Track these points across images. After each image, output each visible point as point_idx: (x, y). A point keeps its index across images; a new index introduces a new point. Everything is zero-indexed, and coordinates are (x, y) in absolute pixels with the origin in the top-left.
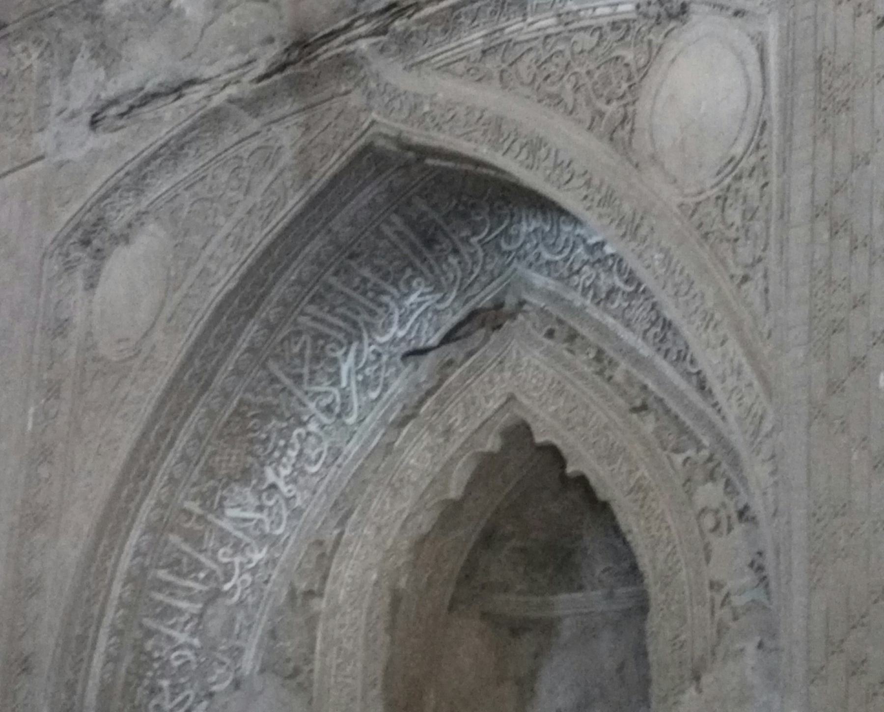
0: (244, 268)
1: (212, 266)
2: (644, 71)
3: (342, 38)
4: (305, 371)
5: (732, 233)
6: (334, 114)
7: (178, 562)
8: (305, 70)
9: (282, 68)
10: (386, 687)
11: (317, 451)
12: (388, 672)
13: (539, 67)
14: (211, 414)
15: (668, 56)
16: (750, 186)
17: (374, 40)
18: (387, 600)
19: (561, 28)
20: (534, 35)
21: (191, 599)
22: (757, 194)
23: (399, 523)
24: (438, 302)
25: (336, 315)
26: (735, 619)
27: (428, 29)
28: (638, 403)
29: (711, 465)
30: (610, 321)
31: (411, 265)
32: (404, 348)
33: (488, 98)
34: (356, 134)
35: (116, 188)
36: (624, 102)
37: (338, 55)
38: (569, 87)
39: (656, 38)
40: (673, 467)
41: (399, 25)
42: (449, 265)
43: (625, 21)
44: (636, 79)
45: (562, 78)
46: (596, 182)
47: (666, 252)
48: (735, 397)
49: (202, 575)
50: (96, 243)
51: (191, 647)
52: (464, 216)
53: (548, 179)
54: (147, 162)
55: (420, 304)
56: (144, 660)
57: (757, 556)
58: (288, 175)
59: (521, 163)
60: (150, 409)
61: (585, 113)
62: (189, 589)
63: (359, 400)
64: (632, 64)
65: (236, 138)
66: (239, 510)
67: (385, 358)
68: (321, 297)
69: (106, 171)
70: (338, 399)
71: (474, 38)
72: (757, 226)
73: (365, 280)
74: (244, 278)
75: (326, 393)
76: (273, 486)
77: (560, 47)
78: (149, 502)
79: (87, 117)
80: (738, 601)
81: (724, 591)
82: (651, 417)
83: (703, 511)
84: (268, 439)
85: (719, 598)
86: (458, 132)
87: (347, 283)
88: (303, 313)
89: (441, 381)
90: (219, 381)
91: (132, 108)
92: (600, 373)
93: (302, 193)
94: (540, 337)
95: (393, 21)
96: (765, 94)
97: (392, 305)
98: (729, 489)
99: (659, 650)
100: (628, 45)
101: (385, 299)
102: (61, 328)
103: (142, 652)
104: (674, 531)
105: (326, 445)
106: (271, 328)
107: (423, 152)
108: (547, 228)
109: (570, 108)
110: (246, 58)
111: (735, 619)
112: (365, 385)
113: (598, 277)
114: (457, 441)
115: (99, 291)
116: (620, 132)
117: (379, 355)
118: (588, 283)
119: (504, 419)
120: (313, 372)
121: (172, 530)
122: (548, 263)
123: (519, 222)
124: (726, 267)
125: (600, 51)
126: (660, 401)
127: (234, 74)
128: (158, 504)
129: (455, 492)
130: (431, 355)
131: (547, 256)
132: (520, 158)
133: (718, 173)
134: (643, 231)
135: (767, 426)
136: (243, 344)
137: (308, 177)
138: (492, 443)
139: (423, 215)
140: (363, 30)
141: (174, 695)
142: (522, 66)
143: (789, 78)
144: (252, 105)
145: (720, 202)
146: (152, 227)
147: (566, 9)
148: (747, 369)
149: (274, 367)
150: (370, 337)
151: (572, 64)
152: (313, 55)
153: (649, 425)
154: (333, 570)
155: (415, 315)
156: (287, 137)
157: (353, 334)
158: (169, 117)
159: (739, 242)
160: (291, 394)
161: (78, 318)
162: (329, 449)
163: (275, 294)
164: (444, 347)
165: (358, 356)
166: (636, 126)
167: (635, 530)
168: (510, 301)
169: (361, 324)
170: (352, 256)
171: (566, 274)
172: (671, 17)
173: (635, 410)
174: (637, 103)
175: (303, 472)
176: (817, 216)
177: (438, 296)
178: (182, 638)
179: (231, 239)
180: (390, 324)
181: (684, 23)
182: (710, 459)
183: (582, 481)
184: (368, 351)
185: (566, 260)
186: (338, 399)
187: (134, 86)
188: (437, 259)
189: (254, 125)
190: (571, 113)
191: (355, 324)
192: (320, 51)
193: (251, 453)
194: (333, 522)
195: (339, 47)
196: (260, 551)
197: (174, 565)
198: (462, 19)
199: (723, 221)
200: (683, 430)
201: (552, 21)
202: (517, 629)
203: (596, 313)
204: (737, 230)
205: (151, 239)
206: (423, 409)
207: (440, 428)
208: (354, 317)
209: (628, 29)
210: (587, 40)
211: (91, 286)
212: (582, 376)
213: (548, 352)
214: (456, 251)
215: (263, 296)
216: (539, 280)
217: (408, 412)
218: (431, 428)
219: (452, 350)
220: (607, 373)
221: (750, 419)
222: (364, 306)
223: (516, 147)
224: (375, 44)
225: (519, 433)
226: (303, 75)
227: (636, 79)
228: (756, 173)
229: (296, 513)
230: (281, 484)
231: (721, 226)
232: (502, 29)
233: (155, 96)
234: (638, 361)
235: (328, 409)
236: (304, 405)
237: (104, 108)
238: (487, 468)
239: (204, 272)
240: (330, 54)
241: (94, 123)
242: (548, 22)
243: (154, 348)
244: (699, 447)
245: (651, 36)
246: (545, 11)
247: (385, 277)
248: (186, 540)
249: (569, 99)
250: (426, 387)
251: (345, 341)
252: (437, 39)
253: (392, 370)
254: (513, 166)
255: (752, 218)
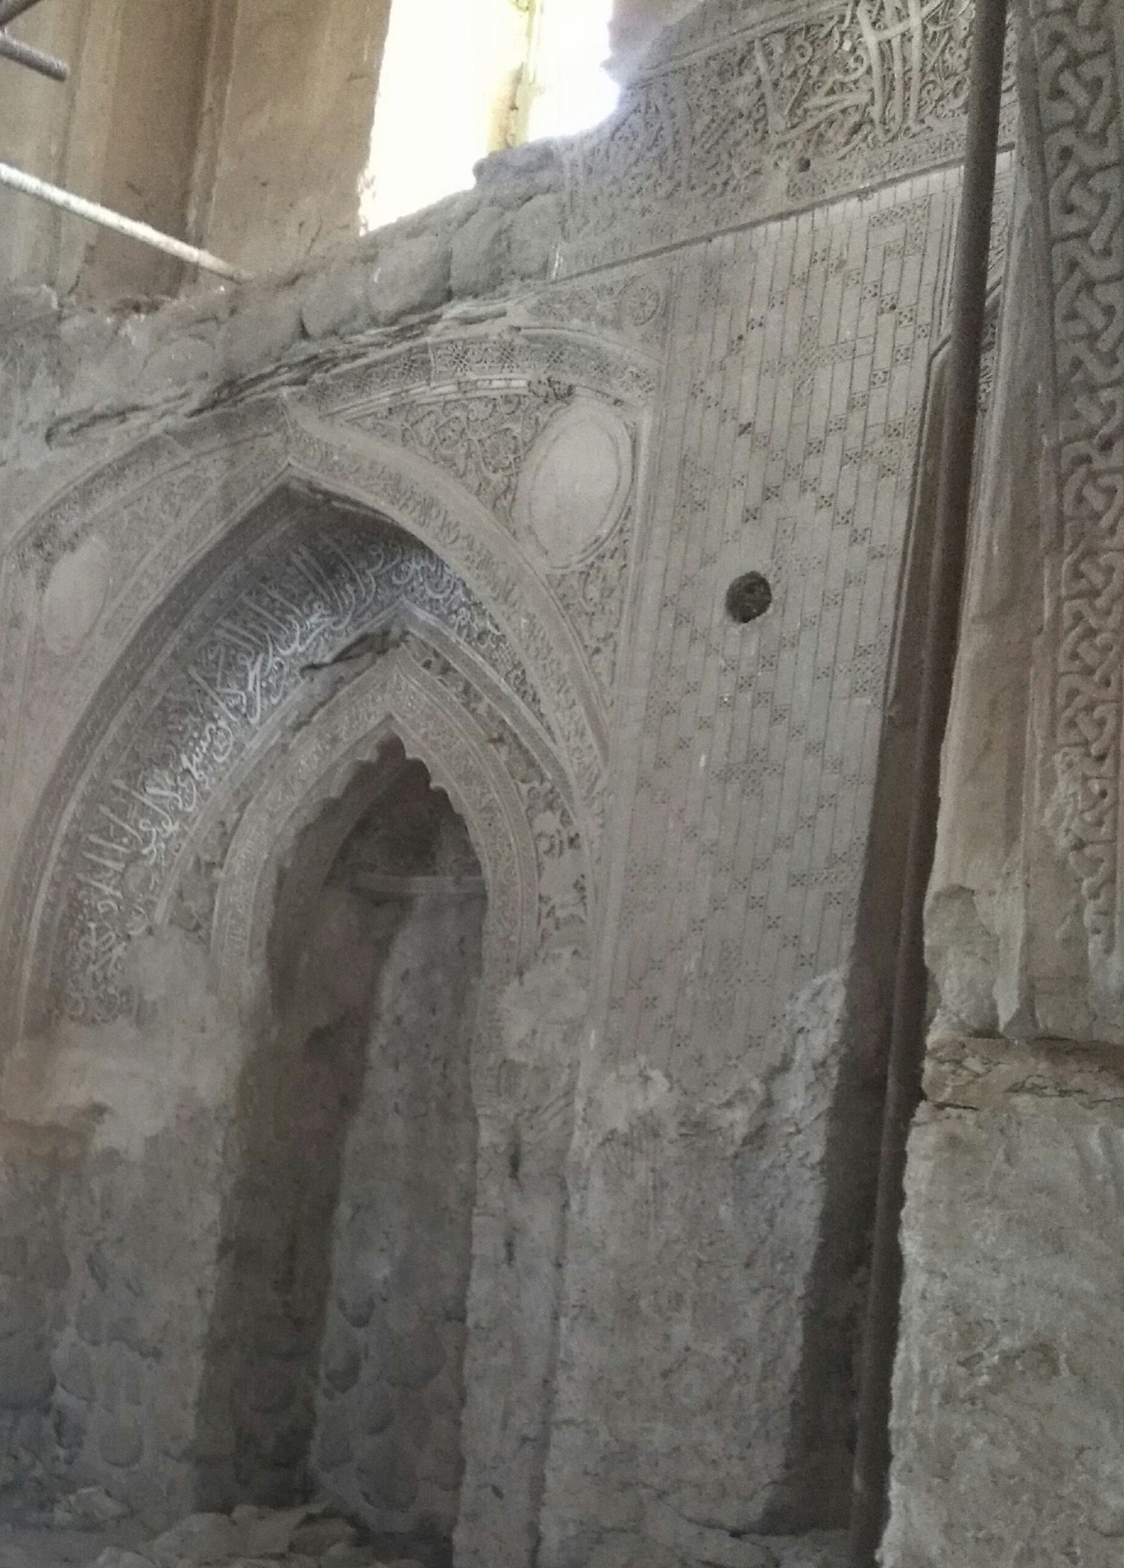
0: (172, 585)
1: (145, 582)
2: (529, 445)
3: (265, 384)
4: (219, 676)
5: (590, 609)
6: (256, 453)
7: (107, 829)
8: (233, 410)
9: (214, 404)
10: (269, 947)
11: (224, 744)
12: (271, 936)
13: (437, 431)
14: (138, 709)
15: (551, 433)
16: (610, 566)
17: (294, 389)
18: (274, 880)
19: (460, 396)
20: (435, 399)
21: (116, 860)
22: (616, 574)
23: (289, 814)
24: (334, 624)
25: (246, 629)
26: (557, 928)
27: (343, 383)
28: (495, 735)
29: (551, 796)
30: (479, 659)
31: (315, 591)
32: (304, 662)
33: (390, 454)
34: (273, 476)
35: (64, 500)
36: (508, 472)
37: (262, 401)
38: (463, 451)
39: (544, 418)
40: (519, 793)
41: (317, 377)
42: (346, 592)
43: (518, 395)
44: (521, 453)
45: (457, 442)
46: (477, 545)
47: (531, 617)
48: (577, 755)
49: (125, 840)
50: (48, 547)
51: (113, 897)
52: (361, 550)
53: (436, 537)
54: (93, 480)
55: (318, 625)
56: (76, 906)
57: (581, 879)
58: (212, 506)
59: (415, 521)
60: (88, 702)
61: (473, 480)
62: (114, 851)
63: (262, 703)
64: (520, 438)
65: (169, 466)
66: (158, 789)
67: (286, 669)
68: (236, 613)
69: (57, 485)
70: (244, 701)
71: (382, 397)
72: (612, 605)
73: (273, 600)
74: (169, 598)
75: (235, 696)
76: (188, 771)
77: (457, 413)
78: (86, 778)
79: (42, 430)
80: (560, 913)
81: (551, 904)
82: (504, 750)
83: (540, 835)
84: (184, 732)
85: (545, 909)
86: (363, 483)
87: (258, 602)
88: (219, 626)
89: (331, 697)
90: (145, 681)
91: (81, 426)
92: (466, 705)
93: (223, 523)
94: (419, 665)
95: (313, 372)
96: (633, 480)
97: (294, 622)
98: (564, 819)
99: (492, 946)
100: (517, 420)
101: (290, 617)
102: (16, 622)
103: (75, 899)
104: (514, 849)
105: (232, 739)
106: (191, 638)
107: (329, 496)
108: (433, 569)
109: (461, 473)
110: (183, 391)
111: (557, 928)
112: (268, 691)
113: (472, 619)
114: (342, 748)
115: (48, 591)
116: (503, 500)
117: (281, 666)
118: (463, 623)
119: (383, 733)
120: (224, 676)
121: (103, 802)
122: (431, 600)
123: (409, 560)
124: (582, 640)
125: (492, 421)
126: (515, 736)
127: (171, 405)
128: (93, 781)
129: (335, 793)
130: (325, 670)
131: (430, 593)
132: (413, 515)
133: (584, 551)
134: (514, 596)
135: (599, 787)
136: (168, 650)
137: (228, 509)
138: (369, 755)
139: (327, 547)
140: (285, 377)
141: (99, 935)
142: (421, 427)
143: (656, 476)
144: (185, 437)
145: (583, 577)
146: (94, 539)
147: (466, 379)
148: (589, 731)
149: (193, 671)
150: (275, 649)
151: (467, 431)
152: (239, 397)
153: (503, 755)
154: (233, 846)
155: (314, 634)
156: (214, 471)
157: (260, 649)
158: (113, 442)
159: (595, 617)
160: (206, 694)
161: (31, 614)
162: (235, 743)
163: (197, 610)
164: (335, 666)
165: (264, 665)
166: (518, 495)
167: (482, 842)
168: (396, 632)
169: (268, 638)
170: (264, 580)
171: (446, 612)
172: (558, 397)
173: (493, 741)
174: (521, 475)
175: (212, 761)
176: (666, 605)
177: (335, 618)
178: (108, 890)
179: (161, 558)
180: (293, 640)
181: (568, 404)
182: (551, 791)
183: (442, 795)
184: (272, 662)
185: (446, 600)
186: (244, 701)
187: (85, 406)
188: (337, 587)
189: (186, 455)
190: (461, 477)
191: (262, 638)
192: (247, 393)
193: (170, 742)
194: (235, 807)
195: (264, 391)
196: (173, 823)
197: (103, 832)
198: (373, 379)
199: (584, 597)
200: (531, 764)
201: (453, 388)
202: (379, 901)
203: (467, 650)
204: (595, 605)
205: (93, 548)
206: (315, 718)
207: (328, 736)
208: (260, 630)
209: (519, 403)
210: (479, 410)
211: (42, 586)
212: (452, 703)
213: (423, 680)
214: (353, 580)
215: (186, 611)
216: (422, 615)
217: (302, 719)
218: (320, 736)
219: (341, 669)
220: (473, 705)
221: (587, 776)
222: (271, 623)
223: (411, 503)
224: (294, 394)
225: (392, 748)
226: (231, 415)
227: (522, 450)
228: (617, 555)
229: (204, 795)
230: (193, 770)
231: (582, 600)
232: (407, 391)
233: (102, 417)
234: (500, 698)
235: (236, 710)
236: (217, 704)
237: (57, 424)
238: (364, 774)
239: (138, 588)
240: (254, 398)
241: (49, 437)
242: (448, 389)
243: (93, 649)
244: (543, 779)
245: (538, 414)
246: (446, 379)
247: (292, 598)
248: (113, 811)
249: (461, 465)
250: (321, 699)
251: (253, 652)
252: (351, 395)
253: (292, 680)
254: (406, 520)
255: (608, 596)
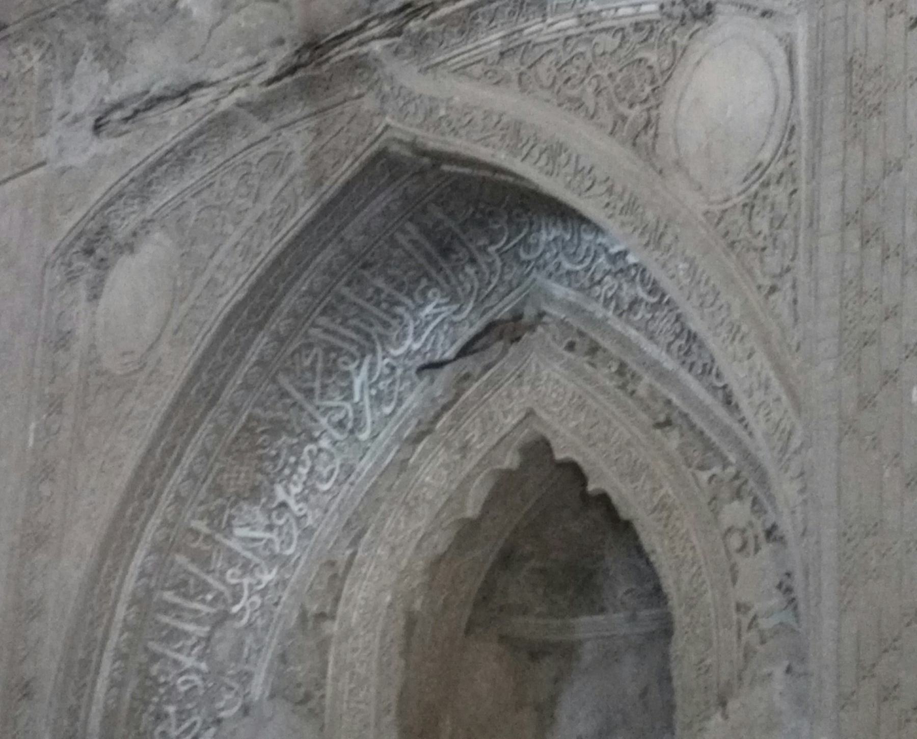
0: (253, 278)
1: (220, 277)
2: (668, 73)
3: (355, 40)
4: (317, 385)
5: (759, 242)
6: (346, 118)
7: (185, 583)
8: (317, 73)
9: (293, 70)
10: (401, 714)
11: (329, 468)
12: (403, 698)
13: (559, 70)
14: (219, 430)
15: (693, 58)
16: (778, 193)
17: (387, 41)
18: (402, 623)
19: (582, 29)
20: (554, 36)
21: (198, 622)
22: (786, 201)
23: (414, 543)
24: (455, 313)
25: (348, 327)
26: (763, 642)
27: (444, 30)
28: (662, 418)
29: (737, 483)
30: (632, 333)
31: (426, 275)
32: (419, 361)
33: (507, 101)
34: (369, 139)
35: (120, 195)
36: (647, 106)
37: (351, 57)
38: (590, 90)
39: (681, 39)
40: (698, 485)
41: (414, 25)
42: (466, 275)
43: (648, 22)
44: (660, 82)
45: (583, 80)
46: (618, 189)
47: (691, 262)
48: (762, 412)
49: (209, 597)
50: (100, 252)
51: (198, 671)
52: (482, 224)
53: (568, 185)
54: (153, 168)
55: (435, 316)
56: (149, 685)
57: (785, 578)
58: (299, 182)
59: (541, 169)
60: (156, 425)
61: (607, 118)
62: (197, 611)
63: (373, 415)
64: (656, 66)
65: (245, 143)
66: (248, 529)
67: (399, 371)
68: (333, 308)
69: (110, 178)
70: (351, 415)
71: (492, 40)
72: (786, 235)
73: (378, 291)
74: (253, 289)
75: (339, 408)
76: (283, 505)
77: (581, 49)
78: (155, 521)
79: (90, 121)
80: (766, 624)
81: (751, 614)
82: (675, 433)
83: (730, 530)
84: (278, 456)
85: (746, 621)
86: (475, 137)
87: (360, 294)
88: (314, 325)
89: (458, 396)
90: (227, 395)
91: (136, 112)
92: (623, 387)
93: (313, 200)
94: (561, 350)
95: (407, 22)
96: (794, 98)
97: (407, 316)
98: (756, 508)
99: (683, 675)
100: (652, 47)
101: (400, 310)
102: (63, 340)
103: (147, 677)
104: (699, 551)
105: (338, 462)
106: (281, 340)
107: (439, 158)
108: (568, 237)
109: (591, 112)
110: (255, 60)
111: (763, 642)
112: (378, 400)
113: (620, 287)
114: (474, 458)
115: (102, 302)
116: (643, 137)
117: (393, 369)
118: (610, 294)
119: (523, 435)
120: (324, 387)
121: (178, 551)
122: (569, 273)
123: (539, 230)
124: (753, 277)
125: (622, 53)
126: (685, 416)
127: (242, 77)
128: (164, 523)
129: (471, 511)
130: (447, 368)
131: (567, 266)
132: (539, 164)
133: (745, 180)
134: (667, 240)
135: (796, 442)
136: (252, 357)
137: (319, 183)
138: (510, 460)
139: (439, 223)
140: (376, 31)
141: (180, 722)
142: (541, 69)
143: (818, 81)
144: (262, 109)
145: (747, 210)
146: (157, 236)
147: (587, 9)
148: (775, 383)
149: (284, 381)
150: (384, 349)
151: (594, 66)
152: (325, 57)
153: (673, 441)
154: (346, 592)
155: (431, 327)
156: (298, 142)
157: (367, 347)
158: (176, 122)
159: (767, 252)
160: (302, 409)
161: (81, 330)
162: (342, 466)
163: (286, 305)
164: (460, 360)
165: (371, 370)
166: (660, 131)
167: (659, 550)
168: (529, 312)
169: (375, 337)
170: (365, 266)
171: (587, 284)
172: (696, 17)
173: (659, 425)
174: (661, 107)
175: (314, 490)
176: (848, 224)
177: (455, 307)
178: (189, 662)
179: (240, 248)
180: (405, 336)
181: (710, 23)
182: (737, 476)
183: (603, 499)
184: (382, 364)
185: (587, 269)
186: (351, 415)
187: (139, 89)
188: (454, 269)
189: (264, 129)
190: (592, 117)
191: (368, 337)
192: (332, 53)
193: (260, 470)
194: (346, 542)
195: (351, 48)
196: (270, 571)
197: (180, 587)
198: (479, 20)
199: (750, 229)
200: (708, 446)
201: (573, 22)
202: (536, 653)
203: (618, 325)
204: (765, 238)
205: (156, 248)
206: (439, 425)
207: (457, 444)
208: (368, 329)
209: (652, 30)
210: (609, 42)
211: (94, 297)
212: (604, 390)
213: (568, 365)
214: (473, 261)
215: (273, 308)
216: (559, 290)
217: (423, 428)
218: (447, 445)
219: (469, 364)
220: (630, 387)
221: (778, 435)
222: (378, 318)
223: (536, 152)
224: (389, 46)
225: (538, 450)
226: (314, 78)
227: (660, 82)
228: (784, 180)
229: (307, 532)
230: (291, 502)
231: (748, 235)
232: (521, 30)
233: (161, 99)
234: (662, 375)
235: (341, 425)
236: (316, 421)
237: (108, 113)
238: (505, 486)
239: (212, 282)
240: (342, 56)
241: (98, 127)
242: (568, 22)
243: (159, 361)
244: (726, 464)
245: (675, 38)
246: (565, 11)
247: (399, 288)
248: (193, 561)
249: (590, 103)
250: (442, 401)
251: (358, 354)
252: (453, 41)
253: (407, 384)
254: (532, 172)
255: (780, 227)
